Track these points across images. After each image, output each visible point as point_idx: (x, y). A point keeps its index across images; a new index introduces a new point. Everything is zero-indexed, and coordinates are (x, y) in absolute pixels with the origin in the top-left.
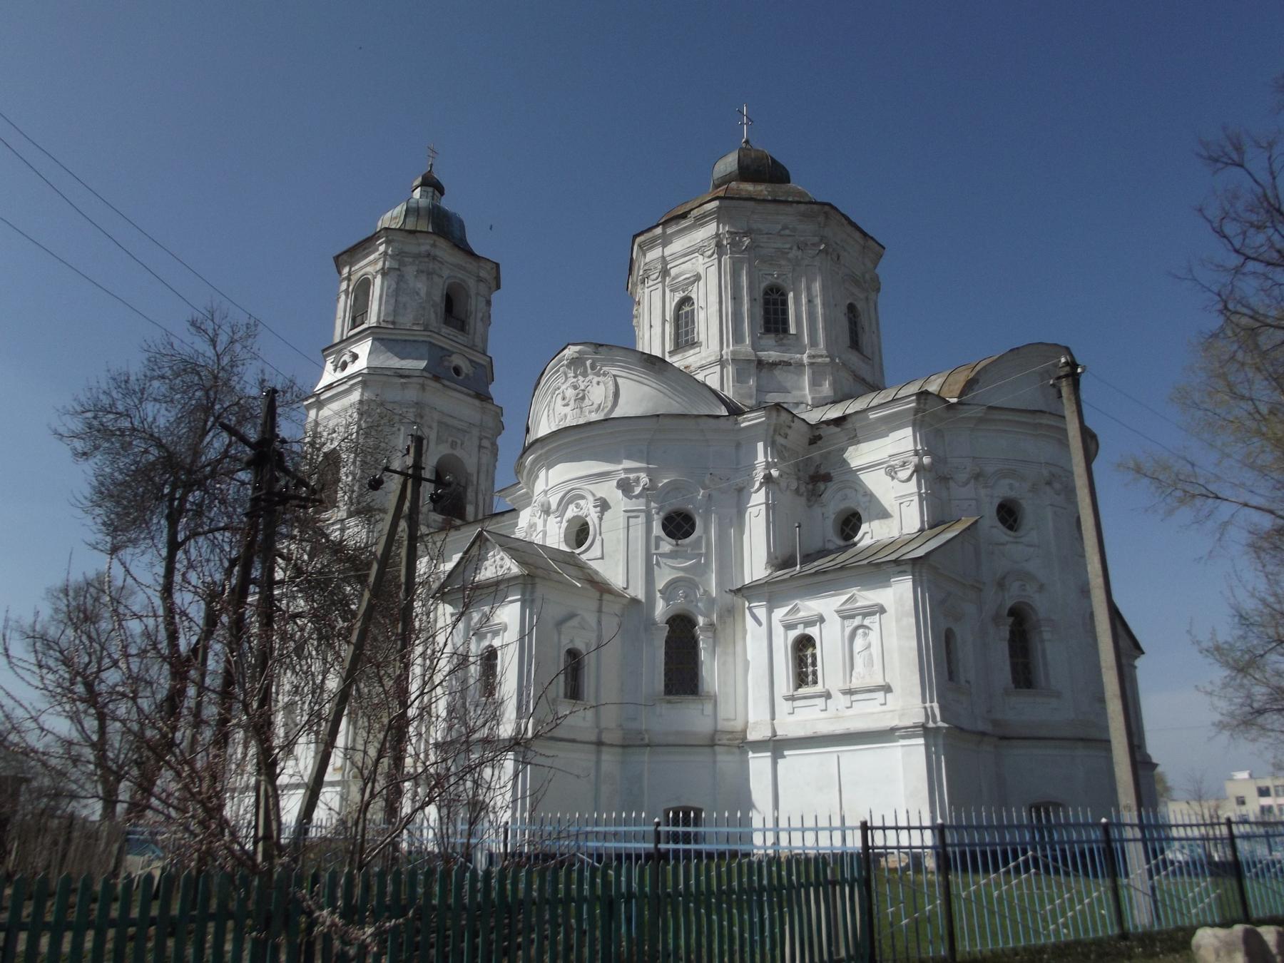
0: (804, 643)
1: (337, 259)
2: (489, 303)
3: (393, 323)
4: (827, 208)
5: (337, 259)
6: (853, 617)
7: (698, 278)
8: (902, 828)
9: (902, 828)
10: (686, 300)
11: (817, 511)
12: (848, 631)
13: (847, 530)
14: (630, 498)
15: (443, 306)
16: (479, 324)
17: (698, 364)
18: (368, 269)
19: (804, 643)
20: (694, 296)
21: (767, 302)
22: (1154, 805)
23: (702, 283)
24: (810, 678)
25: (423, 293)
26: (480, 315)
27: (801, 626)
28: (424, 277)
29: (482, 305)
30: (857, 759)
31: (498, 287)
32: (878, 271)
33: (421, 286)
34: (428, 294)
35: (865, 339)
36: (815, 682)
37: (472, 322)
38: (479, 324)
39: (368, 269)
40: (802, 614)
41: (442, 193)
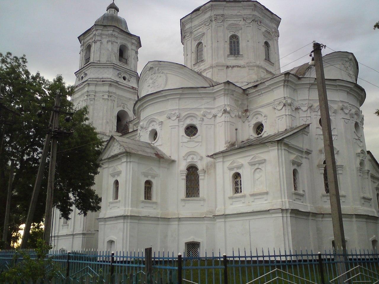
0: (237, 176)
1: (79, 38)
2: (137, 53)
3: (99, 61)
4: (255, 3)
5: (79, 38)
6: (255, 165)
7: (204, 34)
8: (288, 256)
9: (288, 256)
10: (200, 43)
11: (247, 123)
12: (253, 170)
13: (259, 131)
14: (14, 57)
15: (118, 54)
16: (133, 61)
17: (204, 69)
18: (90, 41)
19: (237, 176)
20: (202, 42)
21: (231, 42)
22: (312, 216)
23: (205, 36)
24: (239, 190)
25: (110, 49)
26: (133, 57)
27: (235, 169)
28: (110, 43)
29: (134, 52)
30: (258, 223)
31: (141, 46)
32: (278, 29)
33: (109, 46)
34: (112, 49)
35: (272, 57)
36: (241, 192)
37: (130, 59)
38: (133, 61)
39: (90, 41)
40: (235, 164)
41: (118, 11)
